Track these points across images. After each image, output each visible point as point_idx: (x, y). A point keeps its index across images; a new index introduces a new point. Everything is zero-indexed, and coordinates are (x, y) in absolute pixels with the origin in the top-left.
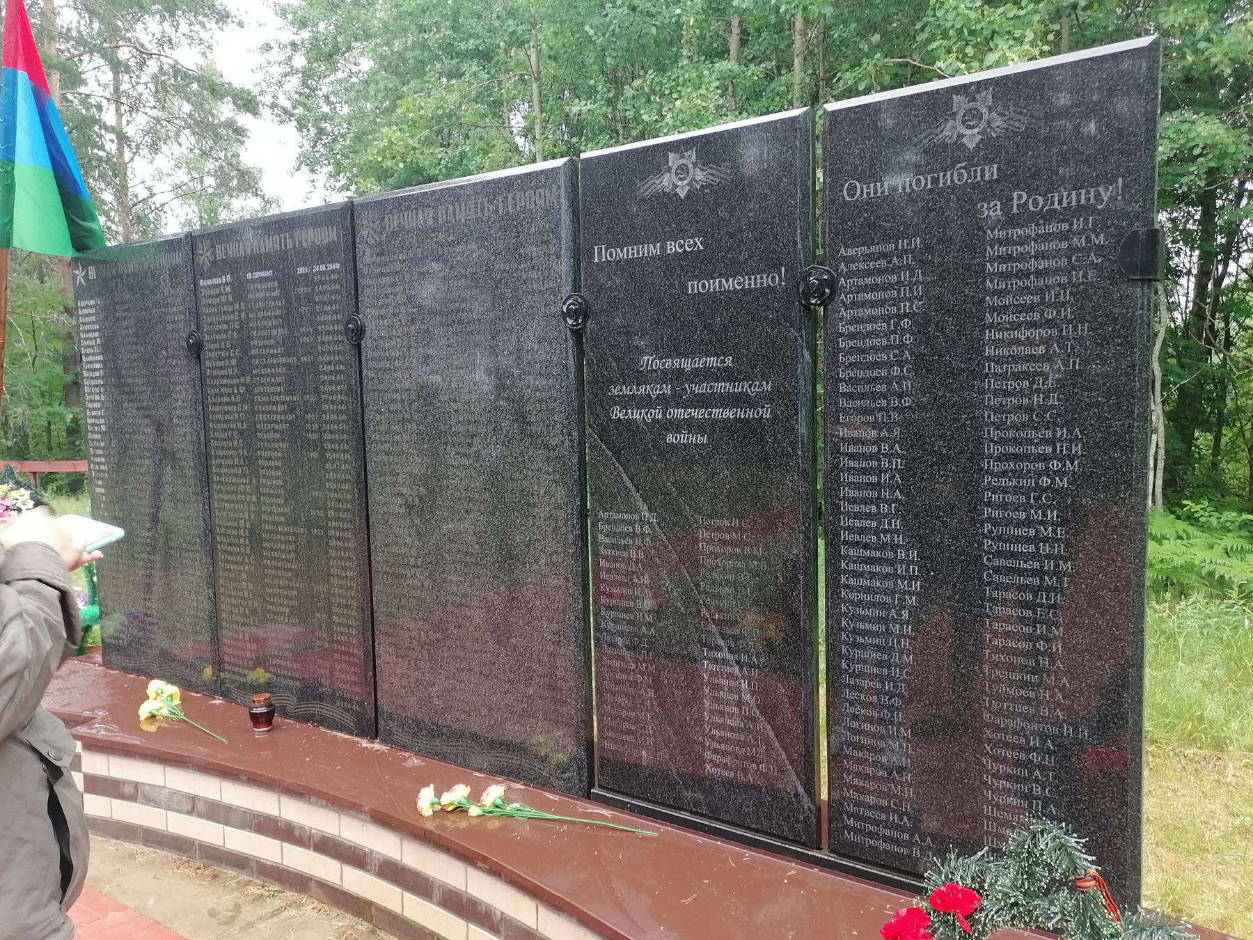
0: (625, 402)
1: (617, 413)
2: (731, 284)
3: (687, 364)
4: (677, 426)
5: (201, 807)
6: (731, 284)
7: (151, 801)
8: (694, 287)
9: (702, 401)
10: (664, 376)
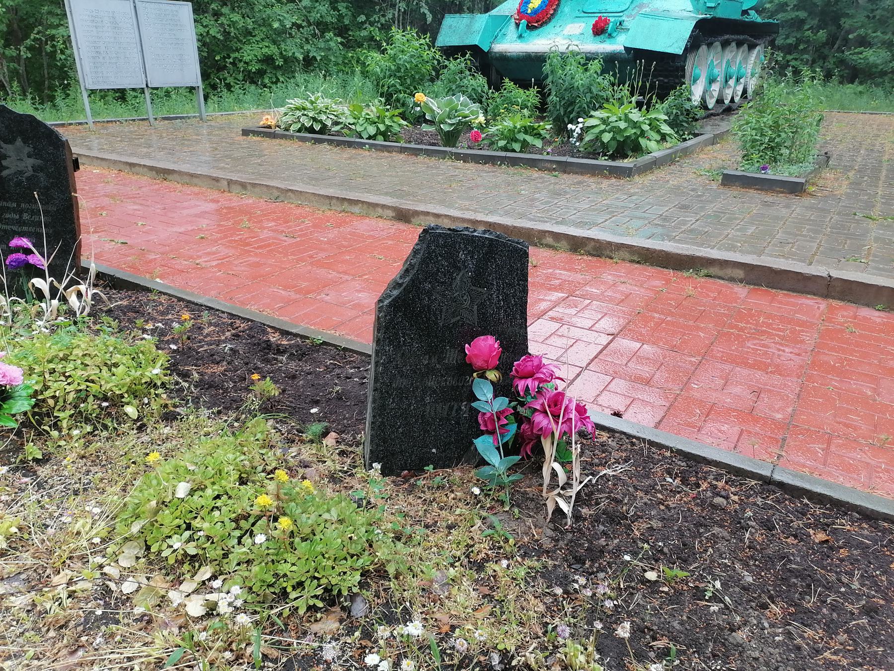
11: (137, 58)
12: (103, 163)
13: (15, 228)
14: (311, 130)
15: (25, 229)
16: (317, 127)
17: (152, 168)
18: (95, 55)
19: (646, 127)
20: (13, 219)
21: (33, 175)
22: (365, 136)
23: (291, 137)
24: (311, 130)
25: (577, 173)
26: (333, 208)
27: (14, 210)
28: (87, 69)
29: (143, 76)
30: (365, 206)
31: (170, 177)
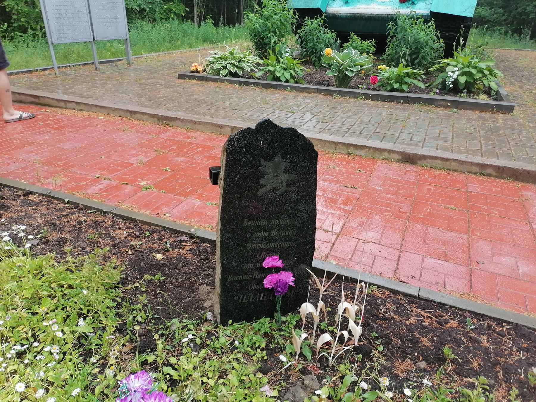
11: (86, 18)
12: (102, 110)
13: (263, 246)
14: (235, 75)
15: (272, 245)
16: (240, 73)
17: (153, 116)
18: (58, 16)
19: (487, 72)
20: (262, 237)
21: (285, 191)
22: (283, 80)
23: (222, 81)
24: (235, 75)
25: (467, 109)
26: (338, 151)
27: (264, 228)
28: (53, 27)
29: (91, 32)
30: (372, 151)
31: (171, 123)
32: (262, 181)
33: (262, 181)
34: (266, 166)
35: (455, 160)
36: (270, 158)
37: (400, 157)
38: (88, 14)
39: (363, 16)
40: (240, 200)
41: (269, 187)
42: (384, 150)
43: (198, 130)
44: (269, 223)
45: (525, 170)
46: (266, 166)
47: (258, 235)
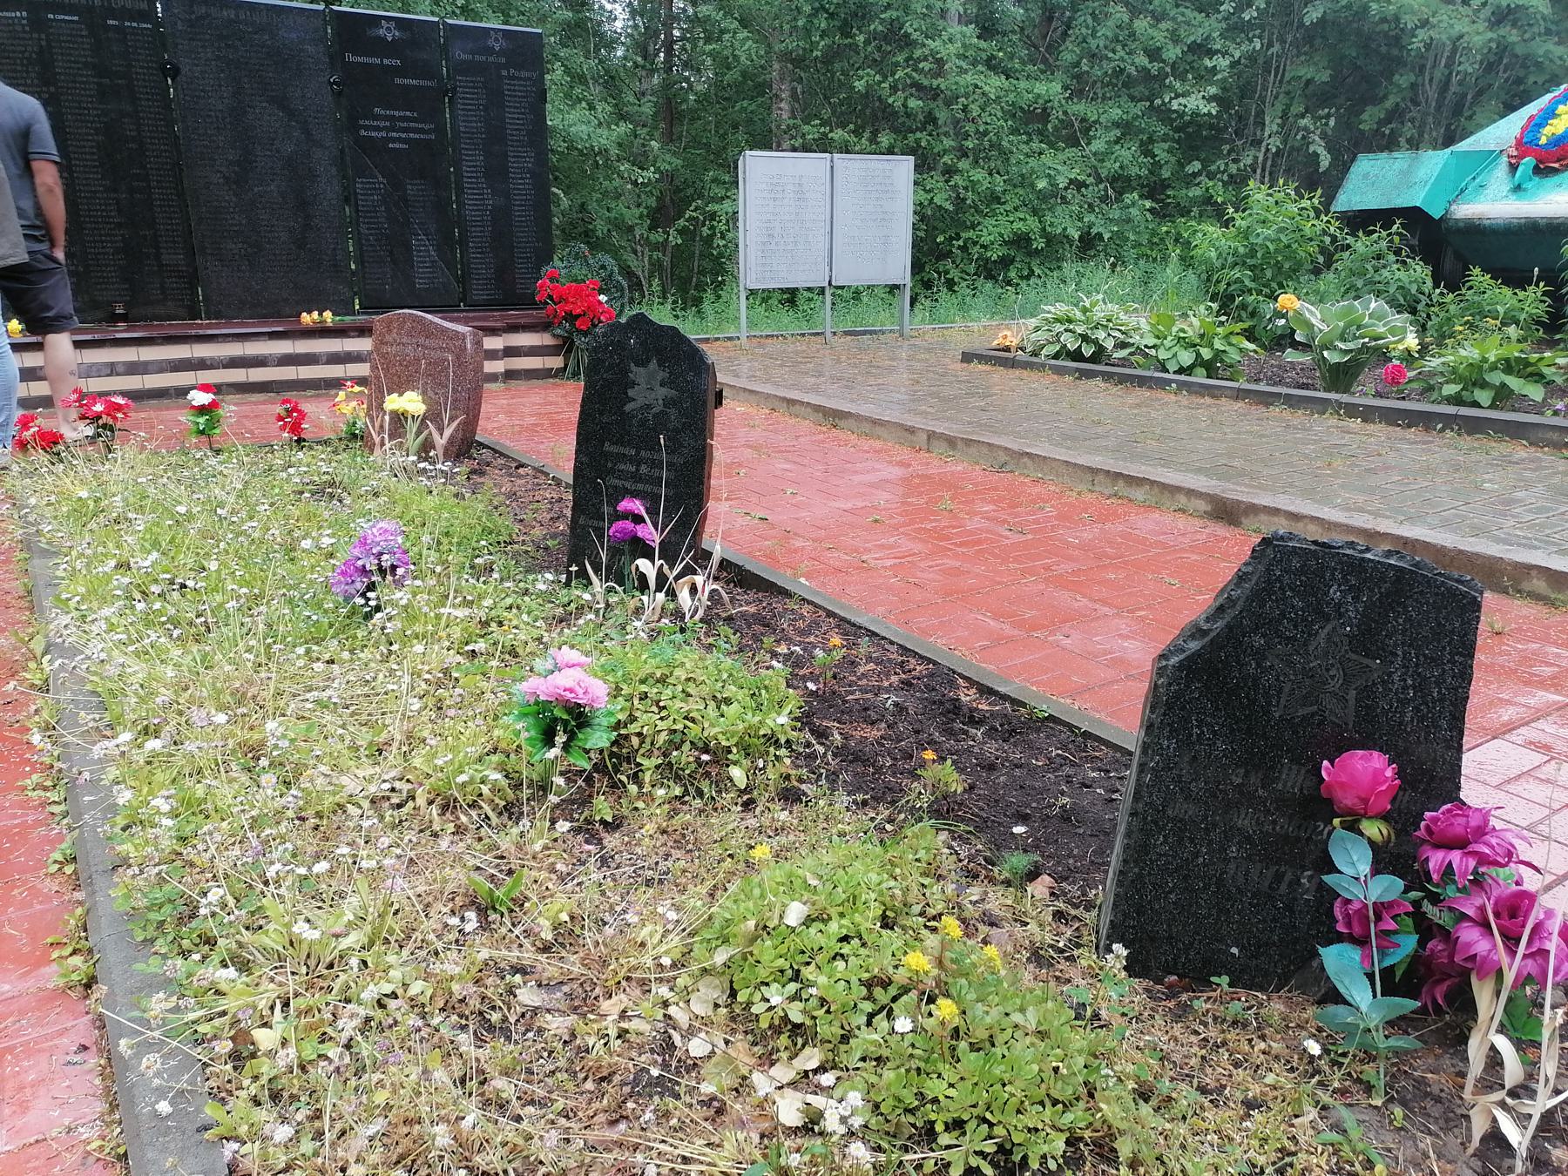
0: (367, 128)
1: (363, 133)
2: (414, 82)
3: (397, 113)
4: (394, 140)
5: (120, 369)
6: (414, 82)
7: (211, 367)
8: (398, 81)
9: (405, 130)
10: (386, 118)
13: (628, 485)
14: (1077, 356)
15: (640, 486)
16: (1088, 351)
17: (818, 408)
22: (1172, 367)
31: (842, 423)
32: (631, 393)
33: (631, 393)
34: (638, 373)
35: (1314, 519)
36: (643, 363)
37: (1209, 508)
38: (828, 237)
39: (1559, 225)
40: (601, 414)
41: (640, 402)
42: (1178, 489)
43: (879, 438)
44: (638, 453)
45: (1461, 552)
46: (638, 373)
47: (622, 467)
